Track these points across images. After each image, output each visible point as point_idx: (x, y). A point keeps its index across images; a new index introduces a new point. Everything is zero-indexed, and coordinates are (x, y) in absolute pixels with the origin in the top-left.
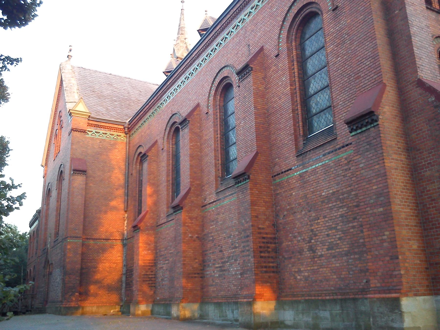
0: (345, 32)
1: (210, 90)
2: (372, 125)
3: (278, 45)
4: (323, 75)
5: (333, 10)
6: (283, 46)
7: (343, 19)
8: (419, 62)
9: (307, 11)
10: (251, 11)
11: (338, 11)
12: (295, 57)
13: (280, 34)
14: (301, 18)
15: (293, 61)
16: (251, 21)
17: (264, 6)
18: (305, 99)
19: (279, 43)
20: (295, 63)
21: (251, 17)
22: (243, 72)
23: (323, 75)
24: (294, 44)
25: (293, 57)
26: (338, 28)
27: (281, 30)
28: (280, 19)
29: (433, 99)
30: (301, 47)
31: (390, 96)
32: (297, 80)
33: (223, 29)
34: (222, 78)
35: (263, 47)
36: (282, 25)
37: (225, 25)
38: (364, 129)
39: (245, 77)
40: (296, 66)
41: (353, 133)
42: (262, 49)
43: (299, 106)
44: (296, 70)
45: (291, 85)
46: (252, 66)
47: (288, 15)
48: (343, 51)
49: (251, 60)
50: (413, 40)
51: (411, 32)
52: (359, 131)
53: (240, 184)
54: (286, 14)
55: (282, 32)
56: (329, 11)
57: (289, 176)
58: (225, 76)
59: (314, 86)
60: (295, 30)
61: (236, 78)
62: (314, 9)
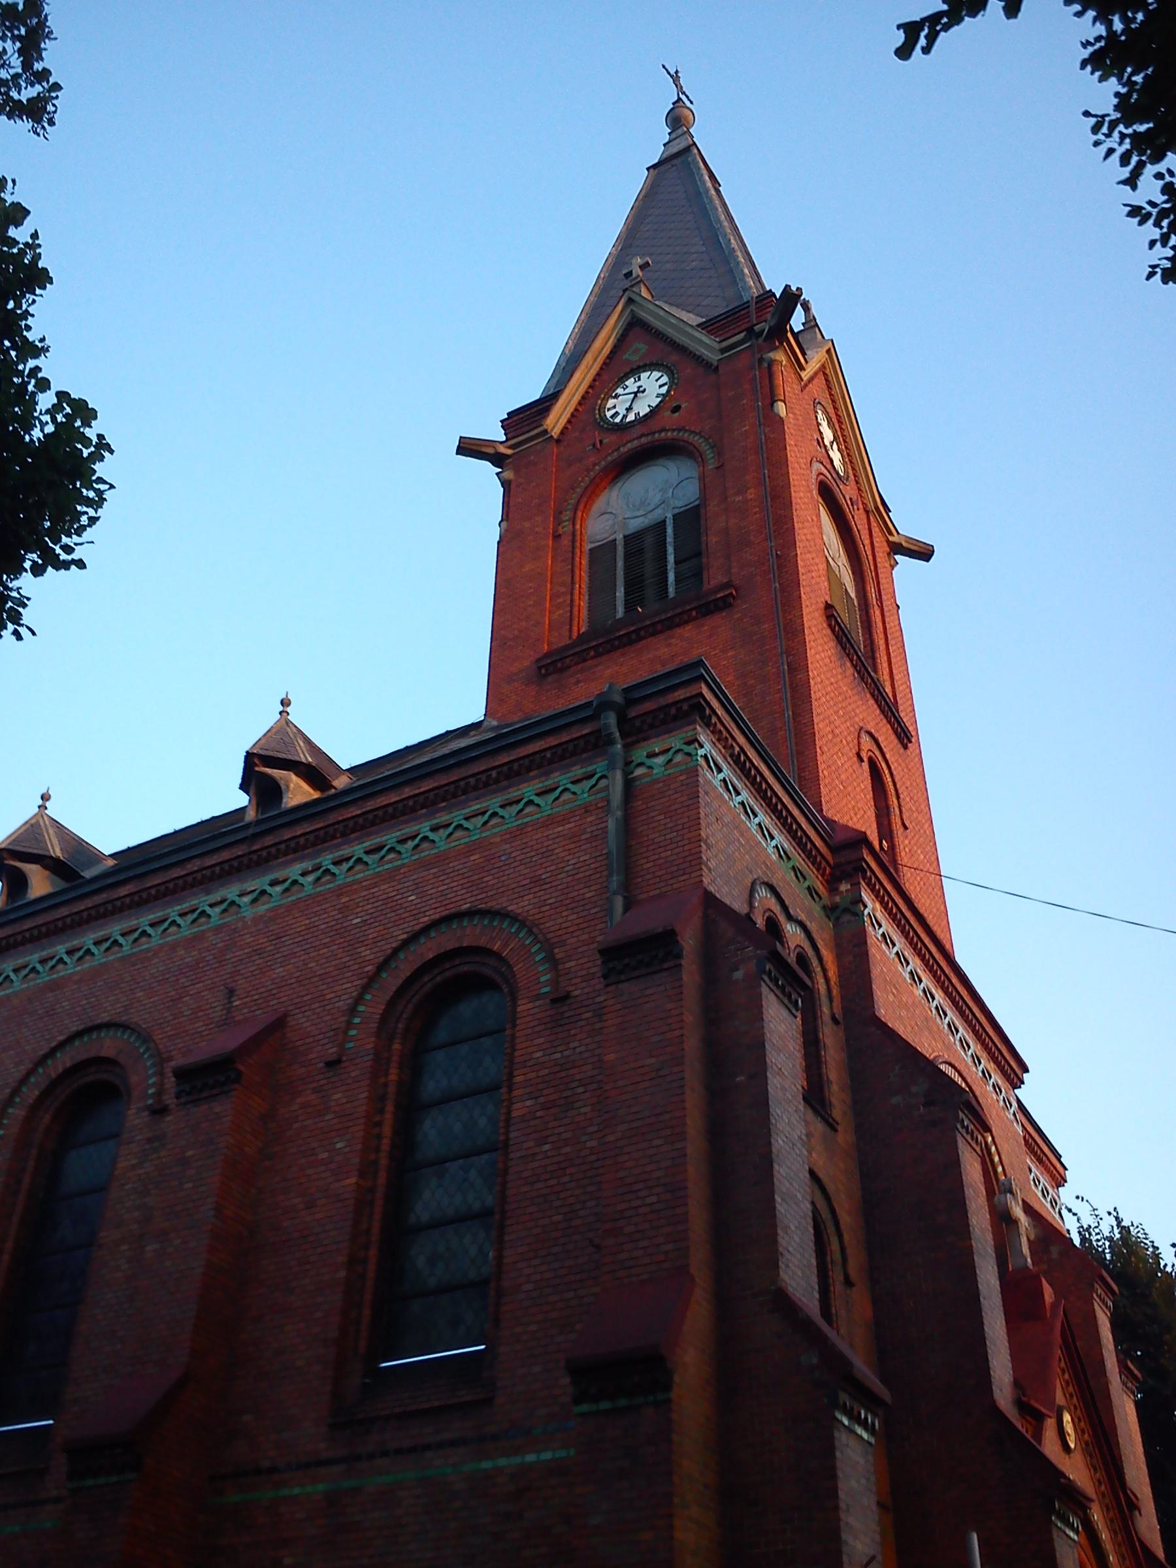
0: (578, 1077)
1: (24, 1080)
2: (651, 1398)
3: (345, 1032)
4: (473, 1174)
5: (554, 1001)
6: (362, 1040)
7: (578, 1037)
8: (783, 1240)
9: (466, 968)
10: (269, 889)
11: (566, 1008)
12: (392, 1089)
13: (359, 999)
14: (438, 979)
15: (383, 1098)
16: (257, 920)
17: (319, 894)
18: (397, 1233)
19: (349, 1025)
20: (390, 1108)
21: (262, 908)
22: (204, 1078)
23: (473, 1174)
24: (396, 1046)
25: (386, 1085)
26: (558, 1055)
27: (366, 988)
28: (370, 955)
29: (815, 1361)
30: (414, 1066)
31: (699, 1314)
32: (384, 1161)
33: (139, 902)
34: (85, 1056)
35: (285, 1015)
36: (373, 978)
37: (153, 892)
38: (622, 1402)
39: (204, 1095)
40: (388, 1117)
41: (584, 1408)
42: (279, 1024)
43: (373, 1252)
44: (387, 1130)
45: (362, 1174)
46: (242, 1068)
47: (402, 955)
48: (562, 1129)
49: (245, 1049)
50: (775, 1173)
51: (774, 1150)
52: (604, 1405)
53: (90, 1482)
54: (396, 951)
55: (368, 997)
56: (538, 997)
57: (285, 1492)
58: (104, 1054)
59: (433, 1198)
60: (410, 1006)
61: (150, 1077)
62: (488, 972)
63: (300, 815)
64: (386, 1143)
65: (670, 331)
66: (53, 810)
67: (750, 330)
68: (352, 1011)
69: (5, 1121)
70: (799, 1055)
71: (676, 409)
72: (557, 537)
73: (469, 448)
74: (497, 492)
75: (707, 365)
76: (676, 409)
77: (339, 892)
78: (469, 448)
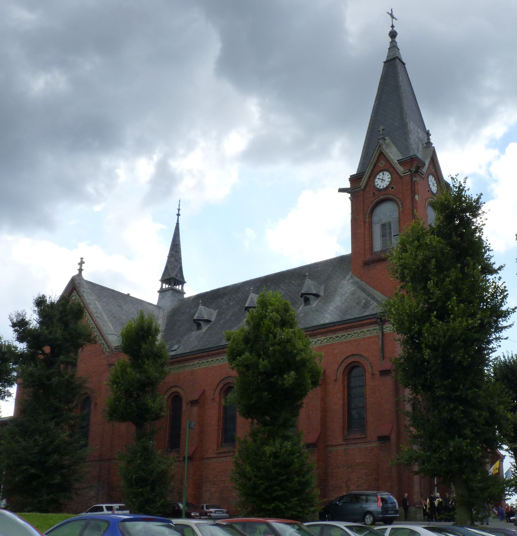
13: (338, 369)
20: (346, 389)
32: (346, 398)
44: (346, 393)
63: (322, 327)
64: (346, 395)
65: (393, 164)
66: (86, 276)
67: (410, 170)
68: (338, 371)
69: (436, 385)
70: (406, 108)
71: (392, 188)
72: (365, 222)
73: (341, 190)
74: (349, 203)
75: (400, 176)
76: (392, 188)
77: (332, 345)
78: (341, 190)
